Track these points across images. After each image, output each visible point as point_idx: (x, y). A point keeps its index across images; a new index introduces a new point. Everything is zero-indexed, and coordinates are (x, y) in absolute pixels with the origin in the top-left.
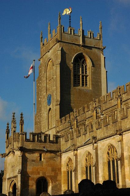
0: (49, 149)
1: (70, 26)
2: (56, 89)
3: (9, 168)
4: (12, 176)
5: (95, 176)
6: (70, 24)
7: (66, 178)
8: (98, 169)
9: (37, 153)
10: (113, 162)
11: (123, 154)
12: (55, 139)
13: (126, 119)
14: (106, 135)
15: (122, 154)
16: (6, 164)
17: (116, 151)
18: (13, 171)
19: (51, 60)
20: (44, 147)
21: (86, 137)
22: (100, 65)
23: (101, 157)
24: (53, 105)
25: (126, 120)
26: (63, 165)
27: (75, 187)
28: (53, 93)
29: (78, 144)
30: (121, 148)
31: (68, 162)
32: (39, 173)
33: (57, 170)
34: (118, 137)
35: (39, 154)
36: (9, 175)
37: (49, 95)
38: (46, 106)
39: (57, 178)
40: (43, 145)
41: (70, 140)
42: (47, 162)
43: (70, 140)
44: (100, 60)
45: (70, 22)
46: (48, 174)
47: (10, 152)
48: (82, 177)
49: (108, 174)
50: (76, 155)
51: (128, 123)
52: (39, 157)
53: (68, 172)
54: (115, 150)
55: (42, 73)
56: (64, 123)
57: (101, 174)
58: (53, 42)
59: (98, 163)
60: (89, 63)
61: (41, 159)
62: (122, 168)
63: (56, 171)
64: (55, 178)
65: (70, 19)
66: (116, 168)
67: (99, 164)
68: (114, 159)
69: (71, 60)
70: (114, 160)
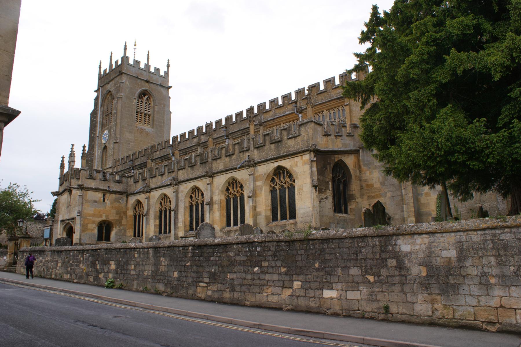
0: (115, 189)
3: (63, 209)
4: (67, 217)
7: (158, 222)
8: (178, 214)
9: (101, 193)
10: (197, 206)
13: (219, 160)
14: (191, 176)
15: (212, 198)
19: (110, 93)
25: (219, 161)
27: (146, 233)
29: (152, 186)
30: (211, 191)
31: (136, 205)
32: (101, 216)
34: (207, 180)
35: (102, 195)
36: (63, 216)
39: (121, 222)
41: (141, 182)
42: (111, 203)
43: (141, 182)
48: (155, 222)
49: (189, 219)
50: (177, 192)
51: (221, 164)
52: (102, 198)
54: (168, 200)
57: (181, 219)
59: (178, 207)
61: (104, 200)
62: (211, 213)
64: (119, 222)
66: (168, 221)
67: (179, 208)
68: (167, 209)
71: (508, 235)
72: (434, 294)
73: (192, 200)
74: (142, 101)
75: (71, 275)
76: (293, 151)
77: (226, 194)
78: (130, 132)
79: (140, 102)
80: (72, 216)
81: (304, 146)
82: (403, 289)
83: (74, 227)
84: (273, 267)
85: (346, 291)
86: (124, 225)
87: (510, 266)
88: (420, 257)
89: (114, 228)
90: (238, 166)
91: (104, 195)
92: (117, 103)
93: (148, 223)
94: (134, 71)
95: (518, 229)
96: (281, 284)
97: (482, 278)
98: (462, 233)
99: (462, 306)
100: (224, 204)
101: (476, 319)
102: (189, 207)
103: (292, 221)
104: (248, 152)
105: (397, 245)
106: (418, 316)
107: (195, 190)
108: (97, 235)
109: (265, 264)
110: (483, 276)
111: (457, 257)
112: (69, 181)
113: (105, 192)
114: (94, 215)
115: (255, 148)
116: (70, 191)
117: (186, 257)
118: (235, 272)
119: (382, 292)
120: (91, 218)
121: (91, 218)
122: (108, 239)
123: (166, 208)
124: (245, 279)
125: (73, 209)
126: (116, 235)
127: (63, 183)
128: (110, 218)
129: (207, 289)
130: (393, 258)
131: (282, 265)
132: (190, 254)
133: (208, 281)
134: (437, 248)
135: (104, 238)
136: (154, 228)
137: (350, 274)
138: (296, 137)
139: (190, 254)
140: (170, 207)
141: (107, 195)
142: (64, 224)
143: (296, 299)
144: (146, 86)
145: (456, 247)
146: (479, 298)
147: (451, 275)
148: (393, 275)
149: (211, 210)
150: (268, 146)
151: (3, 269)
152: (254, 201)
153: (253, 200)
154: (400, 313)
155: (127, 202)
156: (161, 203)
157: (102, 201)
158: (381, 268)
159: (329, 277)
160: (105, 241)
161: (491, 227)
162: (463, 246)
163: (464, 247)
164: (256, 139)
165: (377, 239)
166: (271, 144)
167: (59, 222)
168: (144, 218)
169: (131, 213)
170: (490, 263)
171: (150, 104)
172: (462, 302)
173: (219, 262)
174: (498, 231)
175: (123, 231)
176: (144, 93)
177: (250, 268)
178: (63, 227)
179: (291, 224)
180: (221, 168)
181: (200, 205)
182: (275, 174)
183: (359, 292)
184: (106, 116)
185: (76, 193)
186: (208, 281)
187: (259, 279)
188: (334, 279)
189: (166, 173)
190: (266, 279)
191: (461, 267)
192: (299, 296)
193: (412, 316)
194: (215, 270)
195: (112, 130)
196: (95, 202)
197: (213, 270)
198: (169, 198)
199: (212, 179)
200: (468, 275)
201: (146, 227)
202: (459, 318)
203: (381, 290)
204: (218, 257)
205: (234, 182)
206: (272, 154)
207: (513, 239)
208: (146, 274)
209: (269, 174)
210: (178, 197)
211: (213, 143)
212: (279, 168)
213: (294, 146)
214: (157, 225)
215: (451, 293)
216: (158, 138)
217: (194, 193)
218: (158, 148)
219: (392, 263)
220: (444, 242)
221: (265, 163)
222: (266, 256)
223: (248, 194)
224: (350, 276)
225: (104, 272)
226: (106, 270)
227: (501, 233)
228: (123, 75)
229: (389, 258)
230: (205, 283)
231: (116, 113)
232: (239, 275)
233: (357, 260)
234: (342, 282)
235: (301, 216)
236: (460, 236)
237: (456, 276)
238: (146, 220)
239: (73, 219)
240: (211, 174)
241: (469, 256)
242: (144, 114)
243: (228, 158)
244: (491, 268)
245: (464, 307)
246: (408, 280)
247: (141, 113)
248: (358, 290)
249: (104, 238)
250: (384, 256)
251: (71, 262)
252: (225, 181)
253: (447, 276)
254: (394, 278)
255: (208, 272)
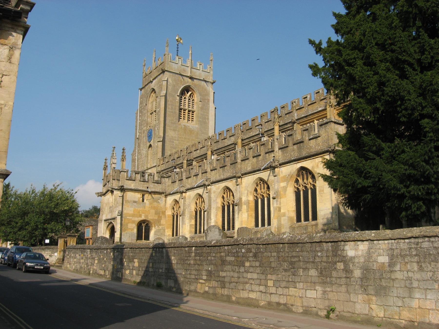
1: (177, 55)
2: (159, 124)
3: (106, 209)
4: (109, 217)
5: (207, 221)
6: (177, 53)
7: (193, 222)
8: (211, 214)
9: (140, 194)
11: (242, 198)
12: (159, 179)
14: (222, 177)
16: (102, 204)
17: (233, 195)
18: (111, 212)
20: (148, 188)
21: (197, 178)
22: (208, 100)
23: (214, 201)
24: (154, 141)
25: (247, 161)
26: (167, 208)
28: (155, 128)
31: (174, 205)
32: (140, 216)
33: (160, 213)
35: (141, 195)
36: (106, 216)
37: (149, 130)
38: (146, 142)
40: (146, 185)
41: (177, 182)
43: (177, 182)
44: (208, 94)
45: (178, 50)
46: (150, 217)
47: (108, 191)
48: (190, 221)
49: (221, 219)
51: (249, 165)
52: (141, 199)
53: (173, 216)
55: (143, 105)
56: (166, 161)
57: (214, 220)
58: (158, 71)
59: (211, 208)
60: (196, 98)
61: (143, 200)
62: (240, 214)
63: (159, 214)
64: (158, 222)
65: (178, 48)
69: (177, 93)
70: (224, 206)
71: (427, 243)
72: (371, 295)
73: (224, 200)
74: (185, 98)
75: (105, 271)
76: (314, 152)
77: (255, 194)
78: (174, 130)
79: (183, 99)
80: (113, 217)
81: (324, 147)
82: (347, 290)
83: (115, 227)
84: (198, 265)
85: (306, 290)
86: (163, 225)
87: (427, 272)
88: (361, 261)
89: (153, 228)
90: (263, 168)
91: (143, 196)
92: (160, 101)
93: (183, 223)
94: (176, 68)
95: (435, 239)
96: (258, 282)
97: (406, 281)
98: (393, 241)
99: (390, 306)
100: (253, 205)
101: (401, 318)
102: (221, 207)
103: (314, 223)
104: (274, 153)
105: (344, 251)
106: (358, 314)
107: (227, 190)
108: (136, 235)
109: (247, 264)
110: (407, 280)
111: (389, 263)
112: (111, 182)
113: (144, 192)
114: (133, 215)
115: (279, 149)
116: (112, 192)
117: (190, 256)
118: (226, 271)
119: (332, 291)
120: (131, 218)
121: (131, 218)
122: (64, 241)
123: (229, 203)
124: (233, 277)
125: (115, 209)
126: (155, 234)
127: (106, 184)
128: (149, 218)
129: (205, 285)
130: (341, 262)
131: (260, 265)
132: (193, 254)
133: (206, 278)
134: (374, 254)
135: (143, 237)
136: (190, 228)
137: (309, 275)
138: (316, 138)
139: (193, 254)
140: (234, 201)
141: (146, 196)
142: (108, 224)
143: (269, 296)
144: (189, 82)
145: (388, 253)
146: (404, 300)
147: (383, 278)
148: (341, 276)
149: (240, 210)
150: (290, 148)
151: (55, 264)
152: (278, 202)
153: (277, 201)
154: (345, 311)
155: (166, 200)
156: (196, 204)
157: (141, 201)
158: (332, 271)
159: (294, 276)
160: (144, 240)
161: (414, 236)
162: (393, 252)
163: (395, 254)
164: (280, 139)
165: (330, 245)
166: (294, 145)
167: (103, 221)
168: (206, 213)
169: (169, 212)
170: (413, 268)
171: (193, 100)
172: (391, 303)
173: (214, 262)
174: (420, 240)
175: (162, 230)
176: (186, 89)
177: (236, 267)
178: (106, 225)
179: (312, 226)
180: (249, 169)
181: (231, 206)
182: (298, 175)
183: (316, 291)
184: (151, 114)
185: (118, 193)
186: (206, 278)
187: (243, 277)
188: (297, 279)
189: (200, 174)
190: (248, 277)
191: (391, 271)
192: (272, 294)
193: (353, 313)
194: (211, 269)
195: (156, 129)
196: (135, 202)
197: (210, 269)
198: (232, 192)
199: (241, 180)
200: (396, 279)
201: (182, 227)
202: (388, 316)
203: (331, 290)
204: (213, 257)
205: (261, 182)
206: (295, 155)
207: (431, 247)
208: (160, 271)
209: (292, 174)
210: (211, 197)
211: (279, 131)
212: (303, 169)
213: (315, 147)
214: (192, 225)
215: (382, 294)
216: (203, 135)
217: (226, 193)
218: (198, 146)
219: (340, 266)
220: (379, 249)
221: (289, 164)
222: (249, 257)
223: (273, 195)
224: (309, 277)
225: (130, 269)
226: (131, 268)
227: (423, 242)
228: (166, 72)
229: (339, 262)
230: (204, 280)
231: (159, 111)
232: (228, 274)
233: (313, 262)
234: (303, 282)
235: (322, 218)
236: (392, 243)
237: (387, 279)
238: (183, 220)
239: (114, 219)
240: (240, 175)
241: (397, 262)
242: (187, 111)
243: (255, 158)
244: (413, 273)
245: (392, 307)
246: (351, 282)
247: (185, 110)
248: (315, 290)
249: (143, 237)
250: (335, 259)
251: (105, 259)
252: (253, 181)
253: (380, 279)
254: (341, 280)
255: (206, 270)
